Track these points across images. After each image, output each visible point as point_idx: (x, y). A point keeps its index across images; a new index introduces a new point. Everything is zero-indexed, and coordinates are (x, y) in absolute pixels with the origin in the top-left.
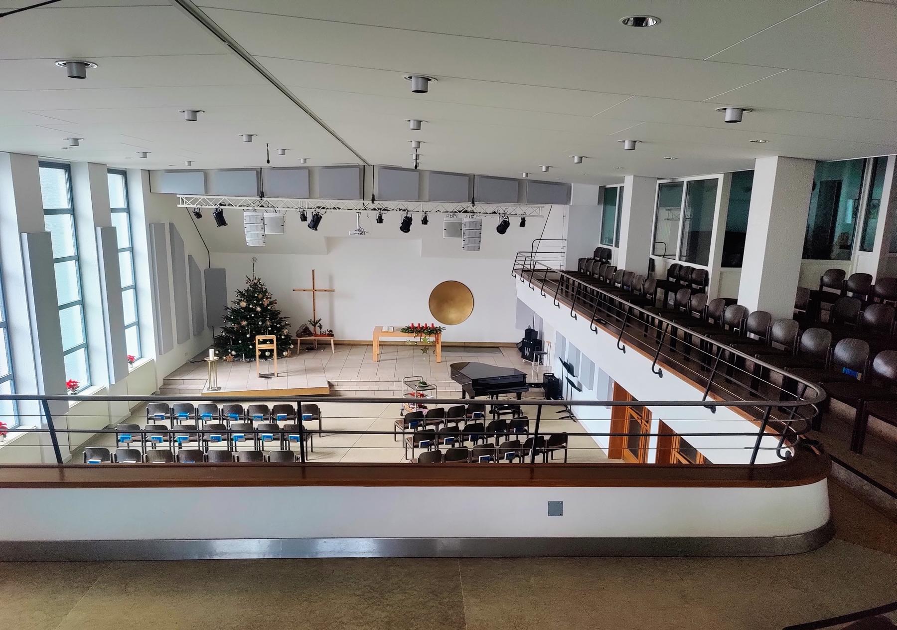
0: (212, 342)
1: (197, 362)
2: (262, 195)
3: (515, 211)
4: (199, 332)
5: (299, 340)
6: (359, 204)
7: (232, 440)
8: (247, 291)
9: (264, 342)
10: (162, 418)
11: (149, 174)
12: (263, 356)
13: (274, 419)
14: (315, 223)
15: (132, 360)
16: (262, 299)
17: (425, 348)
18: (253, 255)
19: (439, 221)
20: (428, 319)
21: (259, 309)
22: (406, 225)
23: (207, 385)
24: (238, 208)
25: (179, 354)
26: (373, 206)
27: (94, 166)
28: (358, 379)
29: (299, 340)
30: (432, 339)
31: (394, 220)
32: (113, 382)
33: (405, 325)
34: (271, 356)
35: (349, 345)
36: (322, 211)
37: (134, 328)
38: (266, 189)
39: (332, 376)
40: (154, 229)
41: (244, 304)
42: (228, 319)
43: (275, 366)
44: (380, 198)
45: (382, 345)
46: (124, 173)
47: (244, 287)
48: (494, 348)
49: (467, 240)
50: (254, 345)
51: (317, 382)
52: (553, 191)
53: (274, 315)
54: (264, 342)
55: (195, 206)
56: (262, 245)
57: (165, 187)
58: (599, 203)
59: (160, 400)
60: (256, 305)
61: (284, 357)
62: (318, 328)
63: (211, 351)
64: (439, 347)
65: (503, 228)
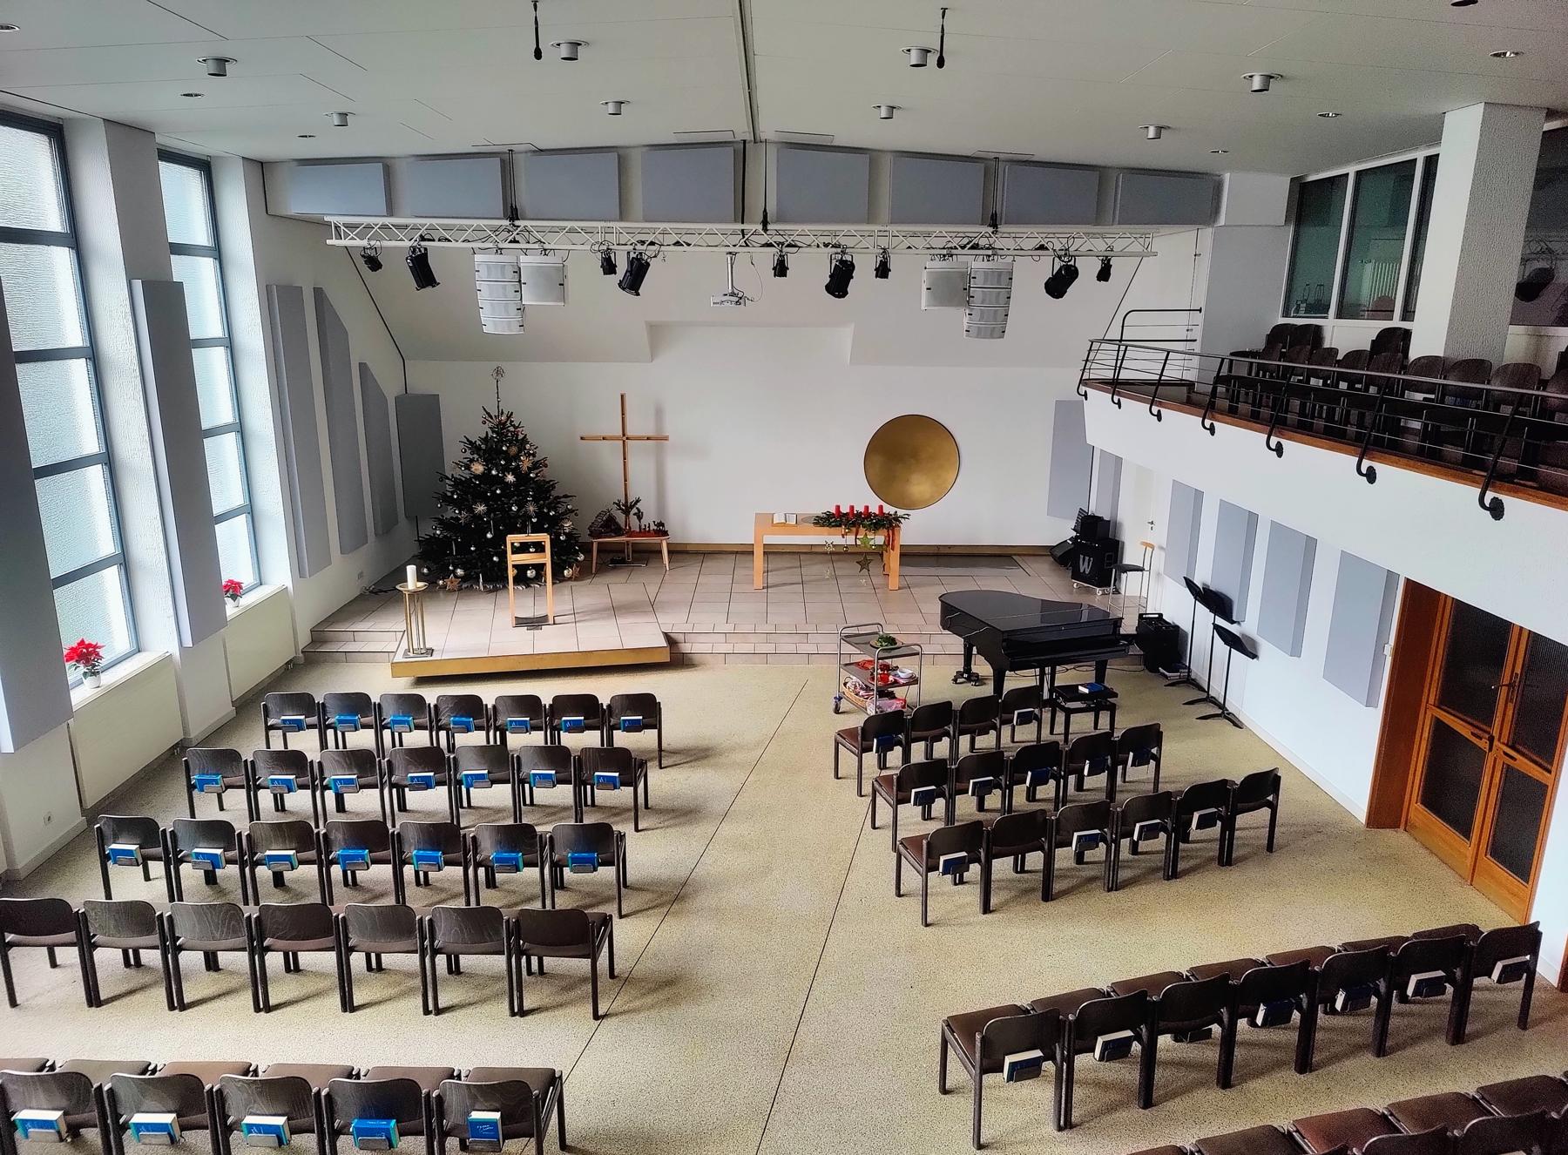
0: (415, 550)
1: (380, 594)
2: (513, 214)
3: (1087, 246)
4: (386, 526)
7: (459, 783)
8: (485, 440)
9: (524, 549)
10: (298, 726)
11: (262, 171)
12: (521, 579)
13: (554, 729)
14: (635, 277)
15: (234, 590)
16: (517, 457)
17: (866, 559)
18: (495, 365)
19: (916, 269)
20: (865, 499)
21: (510, 478)
22: (840, 281)
23: (404, 645)
24: (460, 245)
25: (343, 575)
26: (765, 239)
27: (117, 127)
28: (729, 628)
30: (879, 539)
31: (813, 267)
32: (188, 642)
33: (819, 510)
34: (540, 576)
35: (697, 553)
37: (241, 521)
38: (523, 200)
39: (674, 621)
40: (281, 301)
41: (478, 468)
42: (448, 500)
43: (549, 599)
44: (779, 220)
45: (771, 552)
46: (205, 166)
47: (480, 431)
48: (1003, 557)
49: (977, 312)
50: (503, 555)
51: (644, 635)
52: (1180, 195)
53: (543, 490)
54: (523, 548)
55: (364, 243)
57: (299, 201)
58: (1287, 220)
59: (284, 692)
60: (506, 469)
62: (633, 519)
63: (411, 570)
64: (894, 558)
65: (1058, 285)
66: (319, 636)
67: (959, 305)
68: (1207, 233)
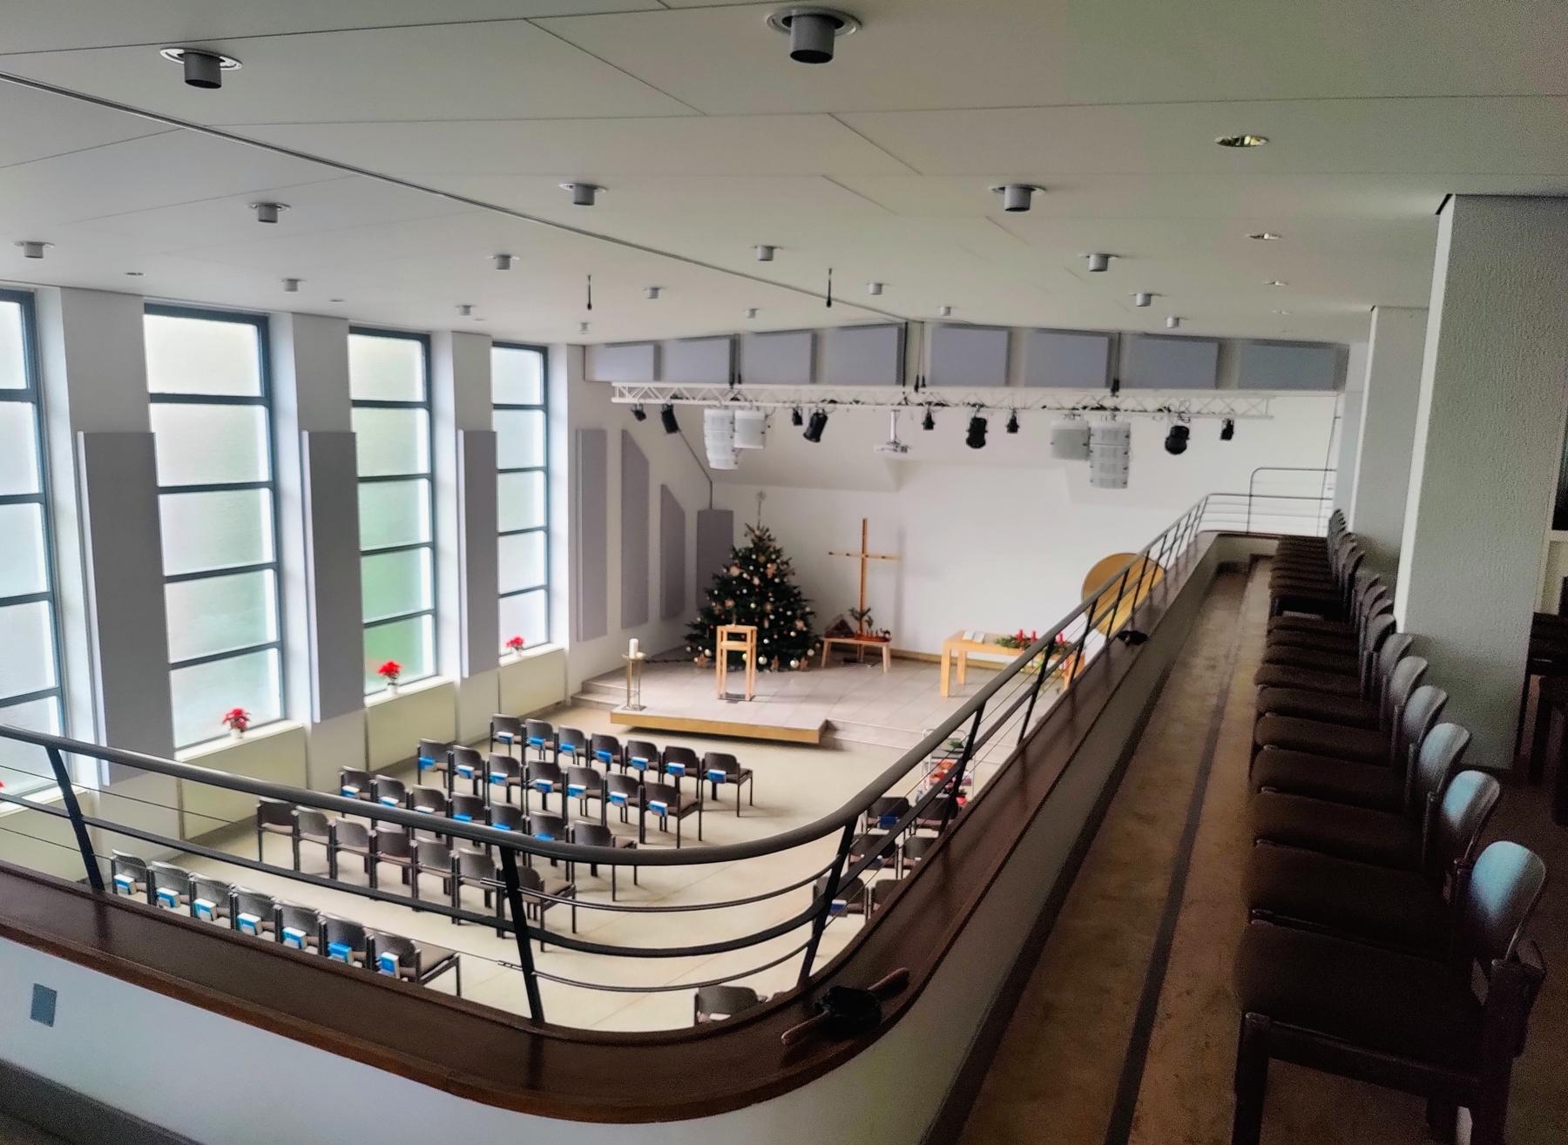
2: (735, 378)
3: (1204, 409)
5: (827, 641)
6: (897, 392)
9: (730, 638)
11: (583, 352)
14: (817, 427)
19: (1041, 425)
22: (977, 434)
29: (827, 641)
31: (955, 424)
32: (466, 675)
36: (828, 407)
38: (746, 367)
39: (835, 714)
40: (588, 445)
41: (735, 571)
43: (749, 681)
44: (934, 383)
54: (733, 636)
56: (732, 466)
60: (751, 574)
61: (791, 669)
62: (865, 626)
66: (586, 688)
67: (1079, 457)
68: (1342, 397)
